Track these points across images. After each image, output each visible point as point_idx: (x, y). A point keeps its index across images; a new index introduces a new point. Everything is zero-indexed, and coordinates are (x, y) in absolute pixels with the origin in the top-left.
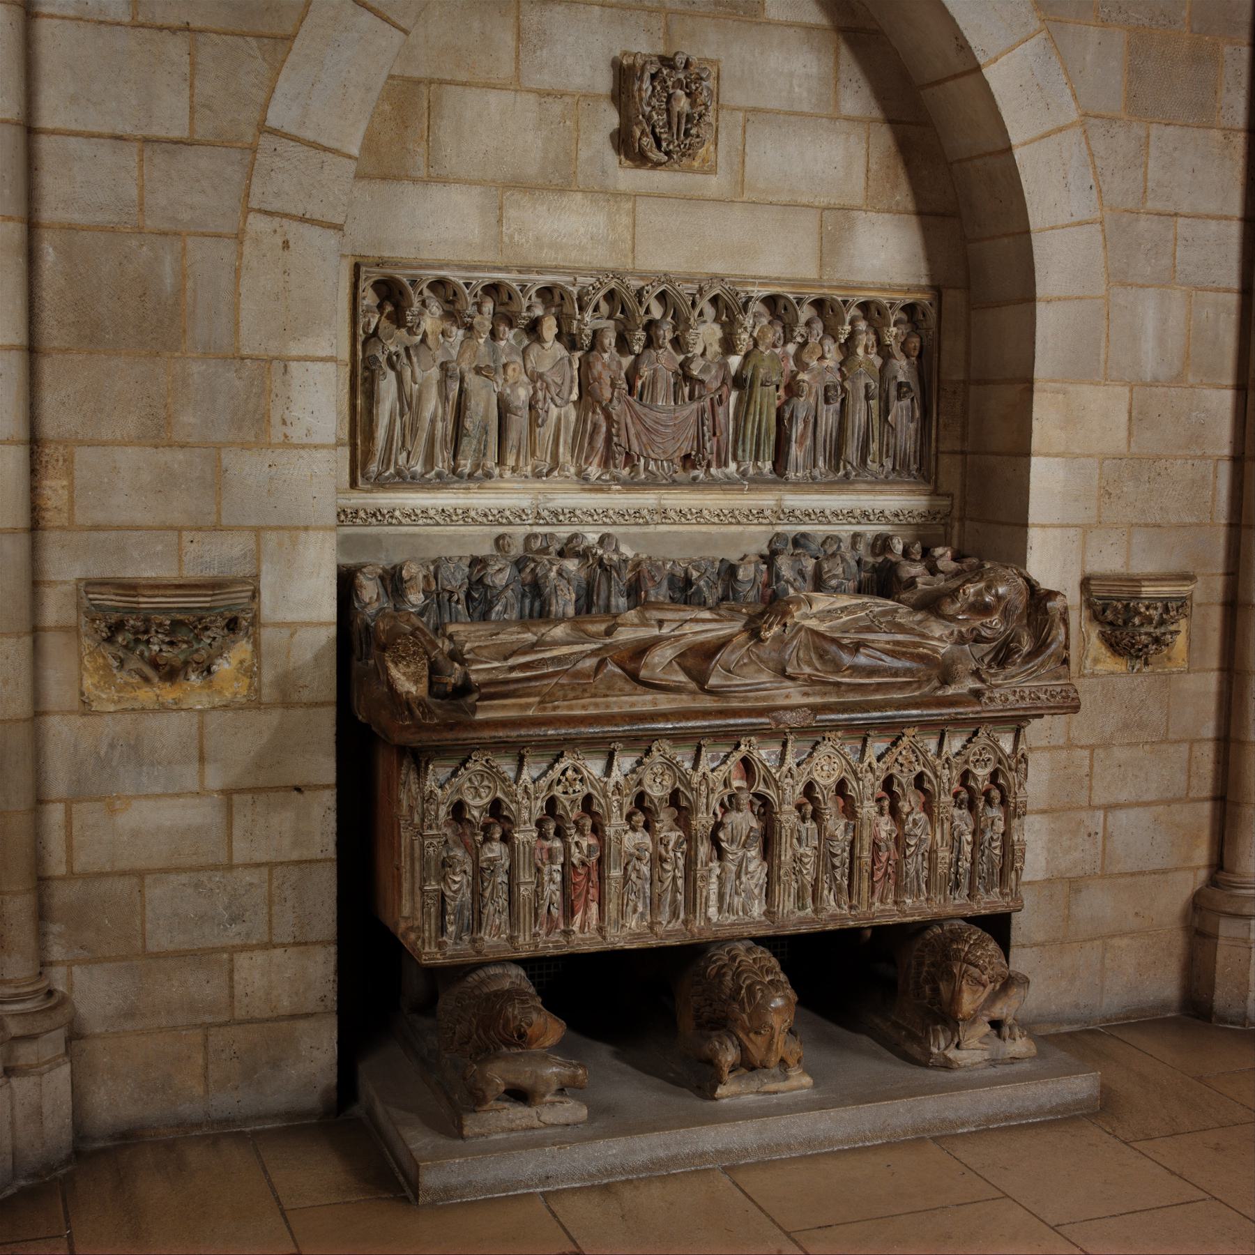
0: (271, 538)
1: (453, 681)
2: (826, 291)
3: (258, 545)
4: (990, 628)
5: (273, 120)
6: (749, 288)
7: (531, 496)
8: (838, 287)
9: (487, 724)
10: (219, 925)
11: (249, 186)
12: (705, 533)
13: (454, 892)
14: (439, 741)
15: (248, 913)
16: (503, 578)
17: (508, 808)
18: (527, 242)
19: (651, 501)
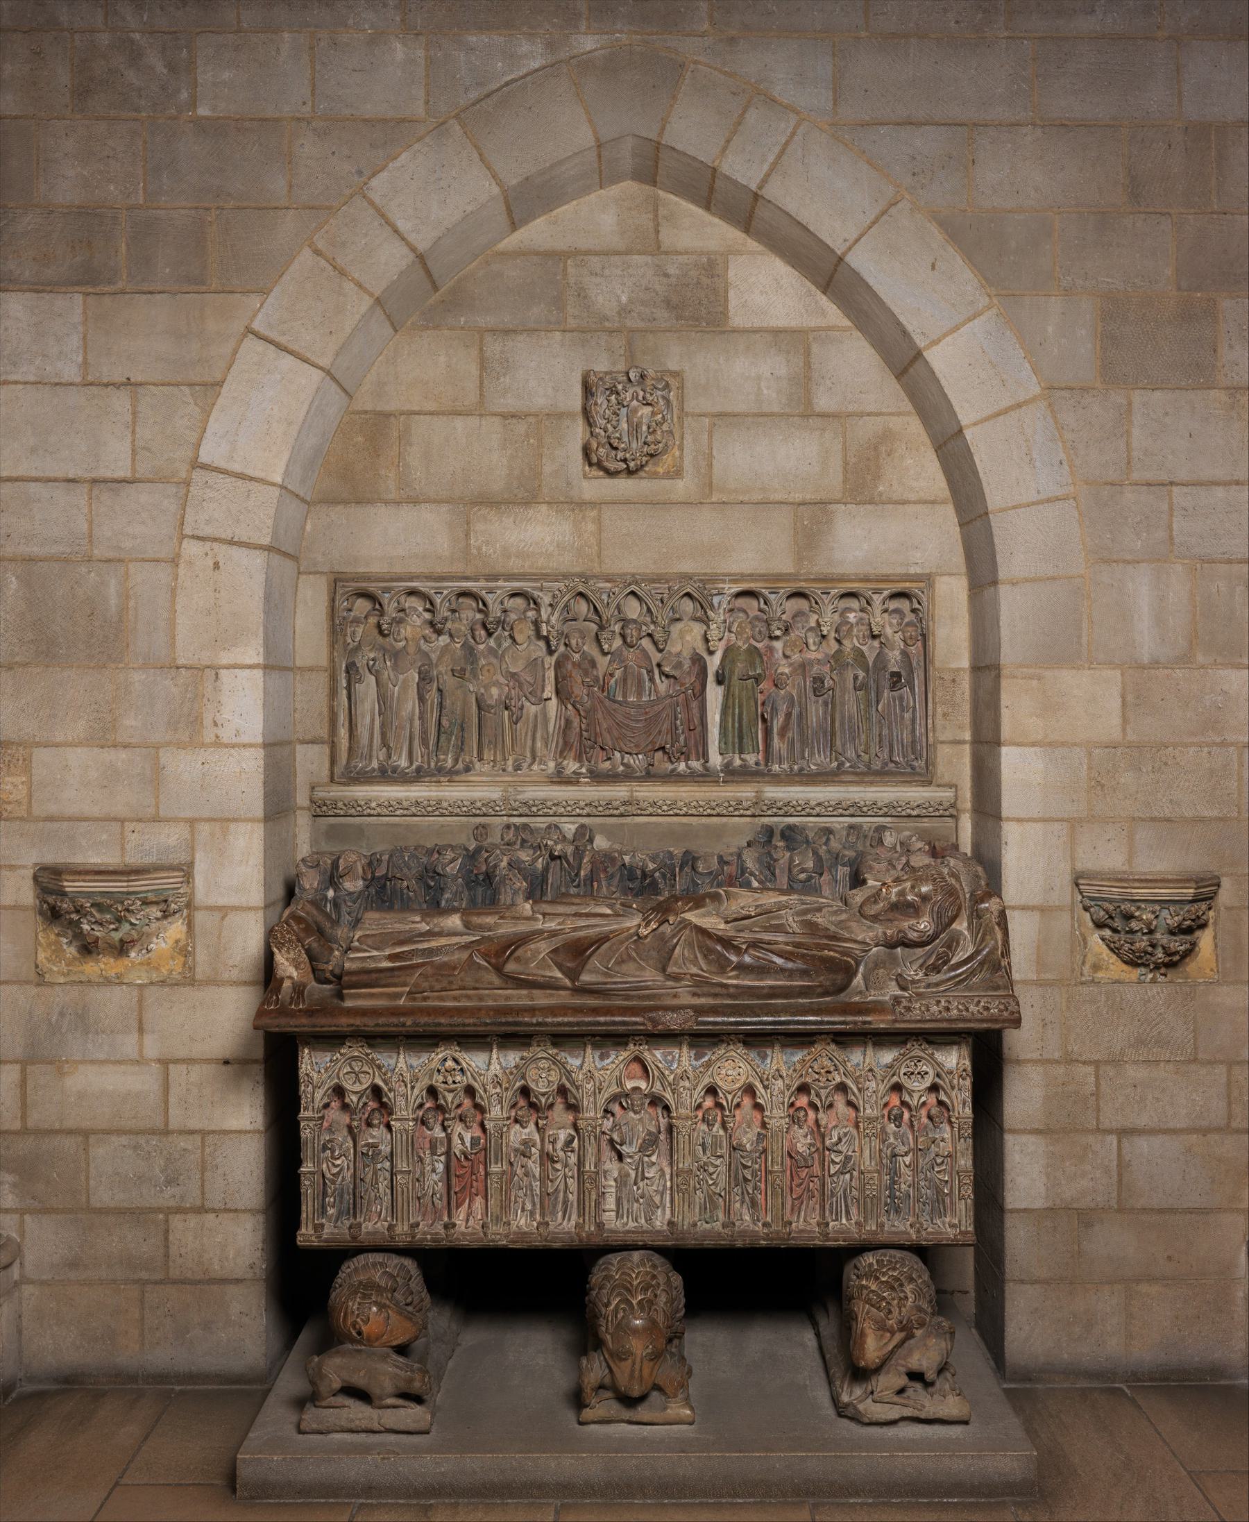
0: (204, 829)
2: (803, 584)
3: (193, 835)
5: (204, 458)
6: (721, 586)
8: (815, 580)
10: (155, 1186)
11: (183, 517)
13: (333, 1175)
14: (296, 1026)
15: (182, 1177)
17: (387, 1096)
18: (495, 553)
19: (621, 794)
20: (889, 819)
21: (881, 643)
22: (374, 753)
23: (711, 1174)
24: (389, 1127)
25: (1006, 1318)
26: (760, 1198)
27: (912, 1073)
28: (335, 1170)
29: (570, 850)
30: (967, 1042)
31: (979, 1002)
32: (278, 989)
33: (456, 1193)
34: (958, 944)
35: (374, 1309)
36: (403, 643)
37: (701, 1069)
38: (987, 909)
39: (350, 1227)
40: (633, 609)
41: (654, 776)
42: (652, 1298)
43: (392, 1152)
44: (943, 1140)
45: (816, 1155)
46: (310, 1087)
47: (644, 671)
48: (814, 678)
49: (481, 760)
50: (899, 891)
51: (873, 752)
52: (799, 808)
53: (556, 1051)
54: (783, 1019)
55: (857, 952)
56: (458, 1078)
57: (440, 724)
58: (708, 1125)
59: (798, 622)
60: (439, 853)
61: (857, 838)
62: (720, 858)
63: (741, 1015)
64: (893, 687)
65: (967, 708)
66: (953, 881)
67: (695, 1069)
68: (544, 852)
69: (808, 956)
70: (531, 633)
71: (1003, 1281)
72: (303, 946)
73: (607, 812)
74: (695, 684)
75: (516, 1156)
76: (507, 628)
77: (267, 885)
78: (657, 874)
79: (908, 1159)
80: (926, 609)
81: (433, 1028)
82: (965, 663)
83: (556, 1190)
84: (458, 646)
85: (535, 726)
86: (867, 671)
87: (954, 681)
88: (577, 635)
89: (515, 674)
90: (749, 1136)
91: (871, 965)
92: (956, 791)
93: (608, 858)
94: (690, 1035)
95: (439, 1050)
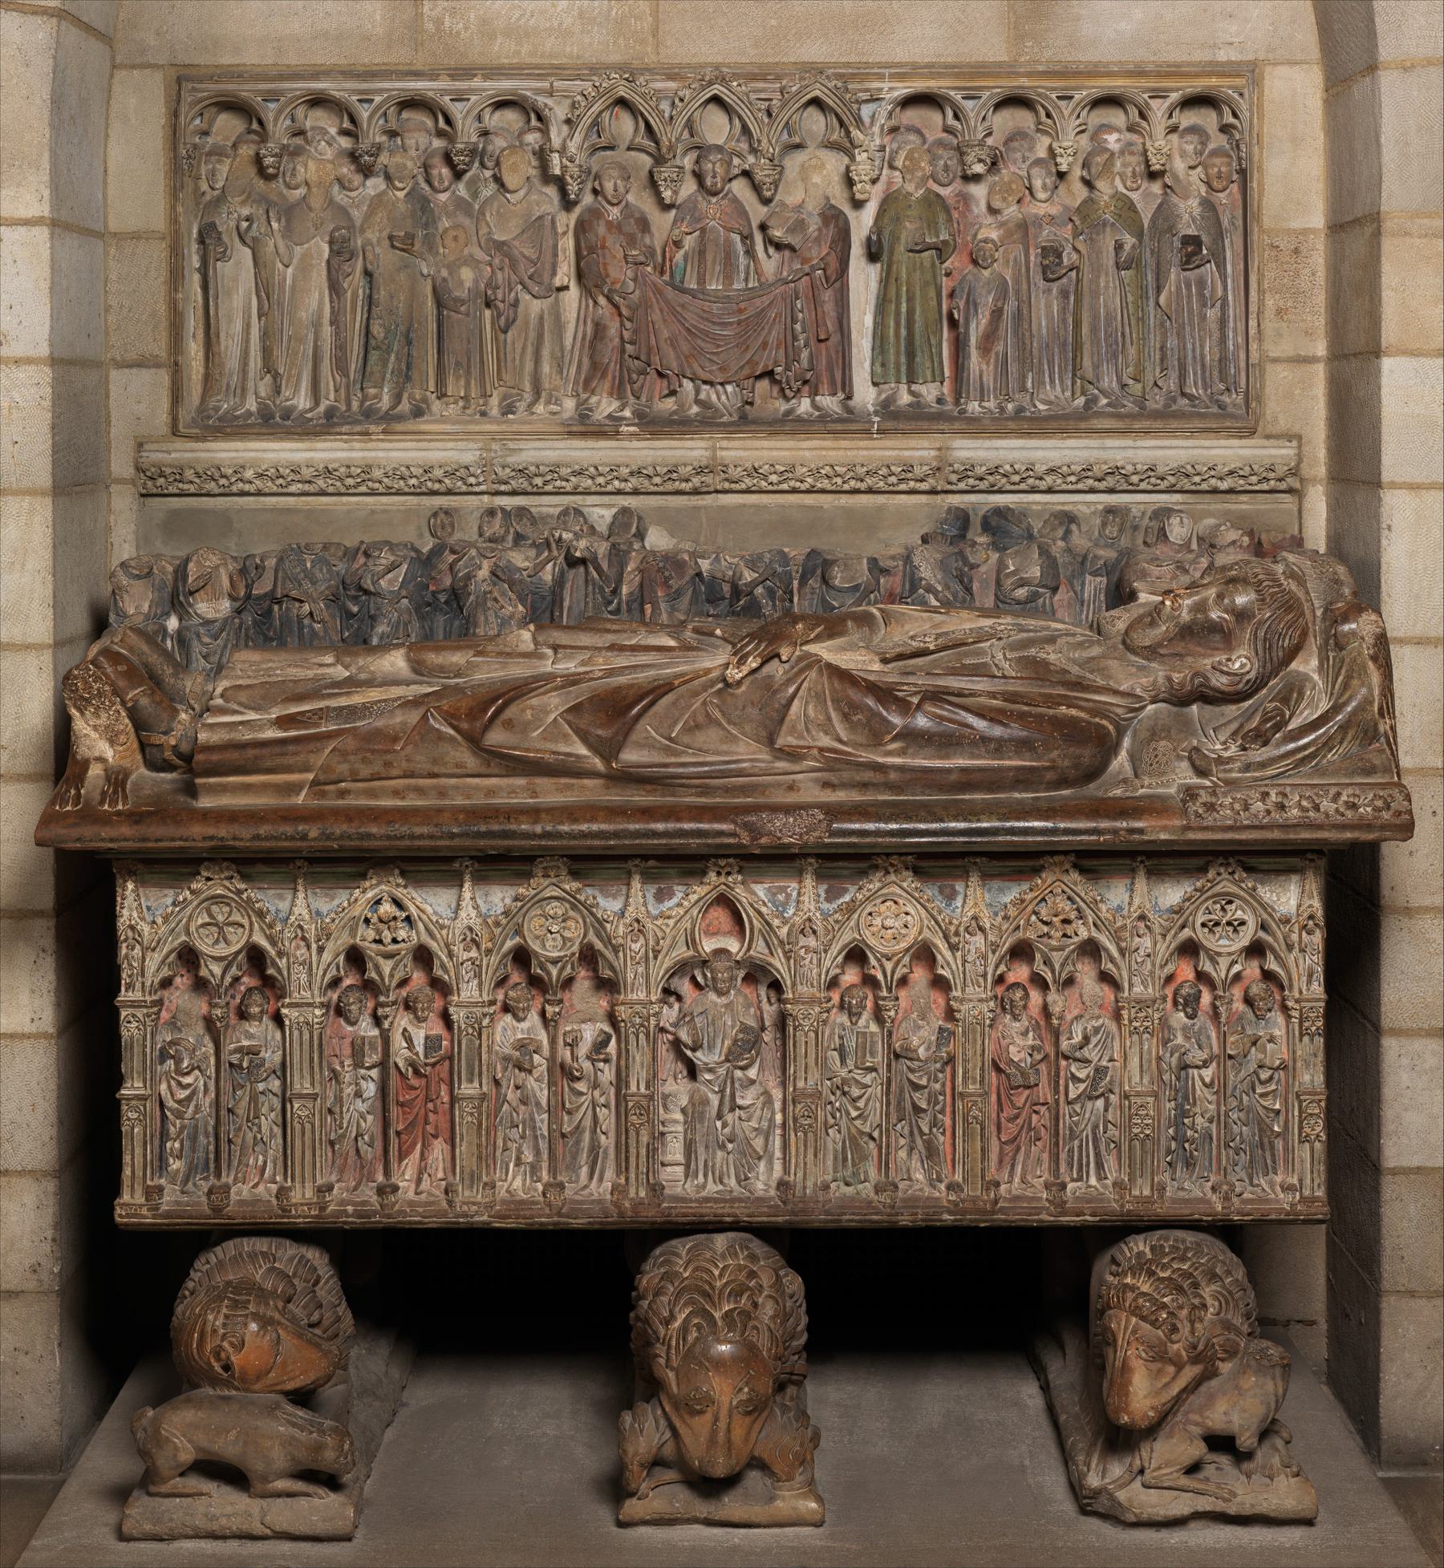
1: (173, 742)
2: (1024, 82)
4: (1228, 674)
6: (875, 85)
7: (480, 445)
9: (206, 816)
12: (811, 507)
13: (179, 1102)
14: (112, 840)
16: (396, 579)
17: (275, 965)
18: (466, 28)
19: (695, 453)
20: (1177, 497)
21: (1166, 186)
22: (250, 384)
23: (854, 1100)
24: (278, 1019)
25: (1383, 1357)
26: (942, 1141)
27: (1217, 924)
28: (182, 1094)
29: (602, 548)
30: (1317, 868)
31: (1339, 794)
32: (80, 778)
33: (398, 1133)
34: (1301, 695)
35: (254, 1326)
36: (301, 191)
37: (837, 916)
38: (1353, 633)
39: (210, 1192)
40: (716, 128)
41: (754, 422)
42: (749, 1307)
43: (283, 1064)
44: (1272, 1040)
45: (1043, 1067)
46: (137, 951)
47: (737, 238)
48: (1043, 248)
49: (442, 396)
50: (1196, 604)
51: (1149, 379)
52: (1016, 478)
53: (575, 885)
54: (985, 825)
55: (1119, 711)
56: (402, 934)
57: (368, 332)
58: (850, 1015)
59: (1014, 150)
60: (367, 555)
61: (1121, 531)
62: (873, 562)
63: (909, 819)
64: (1188, 262)
65: (1320, 299)
66: (1293, 586)
67: (826, 916)
68: (555, 553)
69: (1030, 714)
70: (533, 172)
71: (1378, 1294)
72: (123, 703)
73: (669, 487)
74: (829, 258)
75: (505, 1069)
76: (490, 164)
77: (59, 607)
78: (759, 590)
79: (1208, 1074)
80: (1246, 125)
81: (357, 843)
82: (1317, 219)
83: (577, 1127)
84: (401, 194)
85: (540, 337)
86: (1140, 235)
87: (1296, 251)
88: (615, 173)
89: (503, 243)
90: (924, 1033)
91: (1144, 735)
92: (1300, 447)
93: (672, 561)
94: (818, 856)
95: (367, 884)
